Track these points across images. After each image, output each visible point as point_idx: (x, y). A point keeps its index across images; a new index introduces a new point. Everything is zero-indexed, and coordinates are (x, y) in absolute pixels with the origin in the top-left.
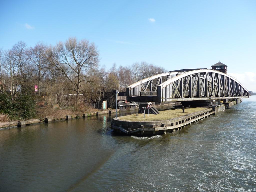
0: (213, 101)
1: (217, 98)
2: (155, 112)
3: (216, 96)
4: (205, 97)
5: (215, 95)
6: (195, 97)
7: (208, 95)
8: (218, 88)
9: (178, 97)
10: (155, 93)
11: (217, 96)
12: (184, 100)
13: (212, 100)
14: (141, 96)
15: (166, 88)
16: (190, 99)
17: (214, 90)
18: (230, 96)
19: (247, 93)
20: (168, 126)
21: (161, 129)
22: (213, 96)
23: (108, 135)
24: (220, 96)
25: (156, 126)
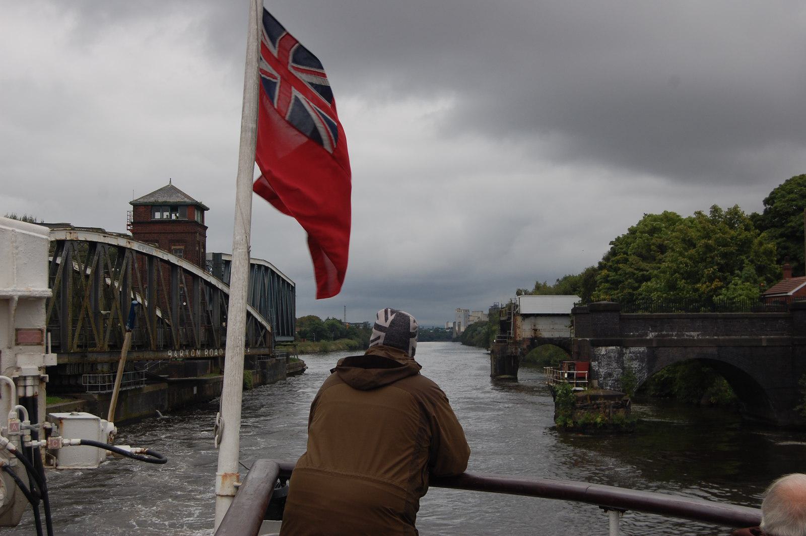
19: (262, 334)
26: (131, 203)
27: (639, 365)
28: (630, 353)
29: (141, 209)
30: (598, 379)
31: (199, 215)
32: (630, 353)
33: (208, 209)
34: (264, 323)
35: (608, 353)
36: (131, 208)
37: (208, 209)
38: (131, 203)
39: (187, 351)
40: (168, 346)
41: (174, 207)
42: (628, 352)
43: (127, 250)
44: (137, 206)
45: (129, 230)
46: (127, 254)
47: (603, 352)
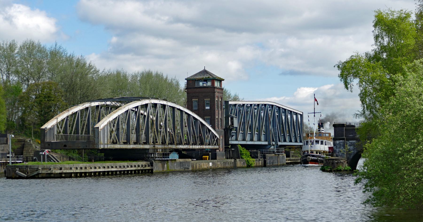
0: (159, 150)
1: (163, 147)
2: (54, 160)
3: (162, 143)
4: (137, 144)
5: (161, 142)
6: (135, 143)
7: (151, 140)
8: (189, 131)
9: (115, 142)
10: (72, 136)
11: (164, 143)
12: (122, 148)
13: (157, 149)
14: (57, 141)
15: (104, 128)
16: (117, 146)
17: (159, 134)
18: (185, 144)
19: (216, 139)
20: (66, 169)
21: (59, 171)
22: (158, 142)
23: (78, 61)
24: (169, 144)
25: (55, 169)
26: (186, 79)
27: (353, 148)
28: (350, 143)
29: (191, 82)
30: (336, 153)
31: (219, 83)
32: (350, 143)
33: (223, 80)
34: (216, 135)
35: (339, 143)
36: (186, 81)
37: (223, 80)
38: (186, 79)
39: (187, 146)
40: (181, 144)
41: (206, 80)
42: (349, 142)
43: (166, 106)
44: (188, 80)
45: (186, 91)
46: (166, 107)
47: (338, 143)
